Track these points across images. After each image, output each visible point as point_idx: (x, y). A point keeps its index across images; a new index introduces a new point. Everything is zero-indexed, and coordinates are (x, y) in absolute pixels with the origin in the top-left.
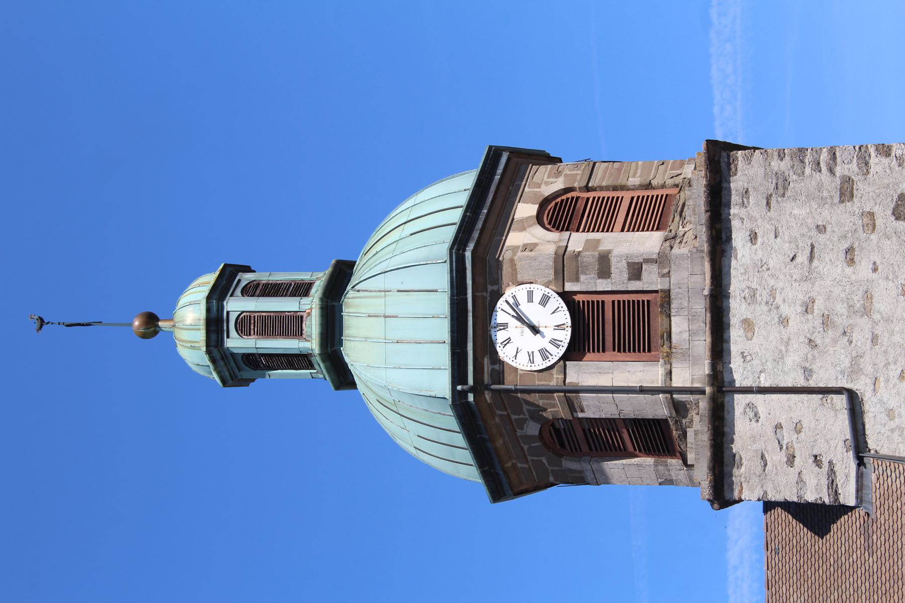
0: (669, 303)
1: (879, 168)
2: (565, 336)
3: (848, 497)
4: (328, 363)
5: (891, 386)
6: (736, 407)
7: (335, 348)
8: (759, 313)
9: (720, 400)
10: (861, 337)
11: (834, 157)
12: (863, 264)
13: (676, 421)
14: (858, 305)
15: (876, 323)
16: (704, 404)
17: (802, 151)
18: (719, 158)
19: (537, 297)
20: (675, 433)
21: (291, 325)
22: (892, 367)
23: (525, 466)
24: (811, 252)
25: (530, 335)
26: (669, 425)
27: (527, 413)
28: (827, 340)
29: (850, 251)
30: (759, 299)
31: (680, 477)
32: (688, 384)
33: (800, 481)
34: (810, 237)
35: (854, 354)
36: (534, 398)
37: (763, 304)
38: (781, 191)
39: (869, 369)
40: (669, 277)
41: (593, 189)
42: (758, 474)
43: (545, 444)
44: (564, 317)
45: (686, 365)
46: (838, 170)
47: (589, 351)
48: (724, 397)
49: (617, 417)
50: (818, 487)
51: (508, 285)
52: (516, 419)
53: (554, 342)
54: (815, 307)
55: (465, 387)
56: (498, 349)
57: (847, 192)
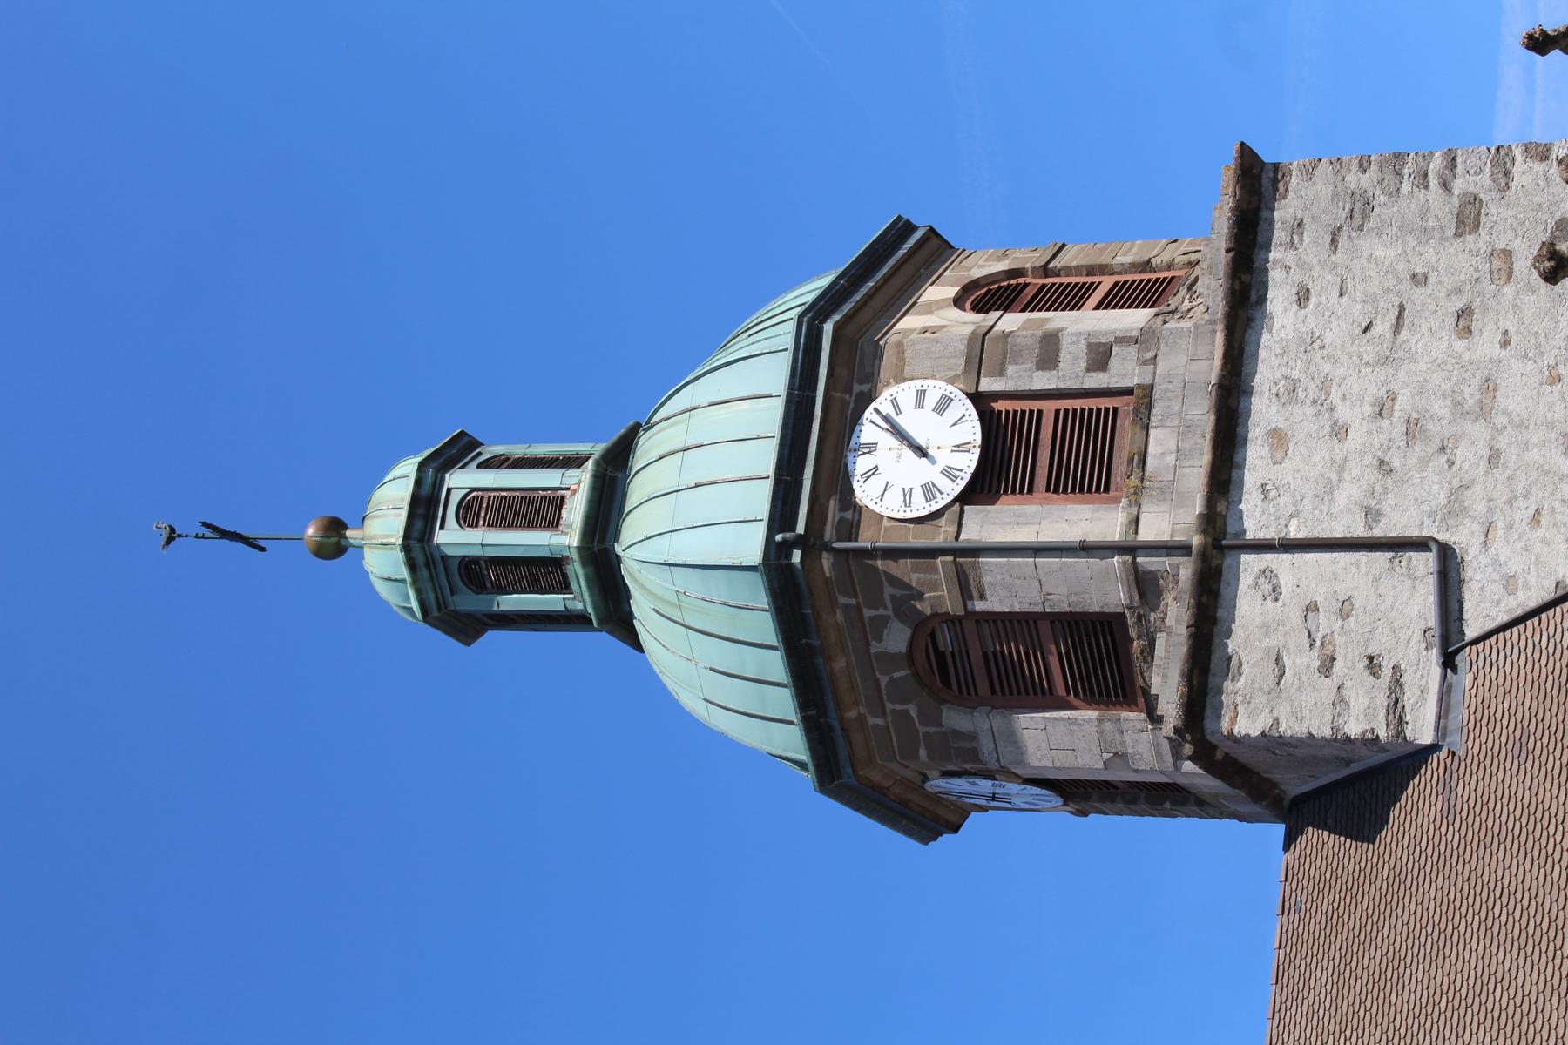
0: (1149, 407)
1: (1526, 180)
2: (968, 463)
3: (1422, 731)
5: (1516, 536)
6: (1242, 576)
8: (1302, 421)
9: (1215, 563)
10: (1469, 455)
11: (1452, 164)
12: (1485, 333)
13: (1140, 617)
14: (1471, 402)
15: (1499, 431)
16: (1186, 570)
17: (1399, 157)
18: (1256, 184)
19: (931, 400)
20: (1136, 646)
21: (541, 510)
22: (1521, 503)
23: (880, 721)
24: (1398, 318)
25: (918, 447)
26: (1126, 627)
27: (890, 605)
28: (1412, 461)
29: (1464, 314)
30: (1301, 395)
33: (1340, 700)
34: (1400, 293)
35: (1456, 483)
36: (903, 569)
38: (1357, 220)
39: (1479, 508)
42: (1266, 688)
43: (916, 674)
44: (972, 431)
45: (1165, 507)
46: (1458, 185)
47: (1006, 492)
48: (1223, 558)
49: (1039, 609)
50: (1369, 712)
52: (872, 618)
53: (949, 473)
54: (1397, 407)
55: (788, 535)
56: (855, 485)
57: (1469, 218)
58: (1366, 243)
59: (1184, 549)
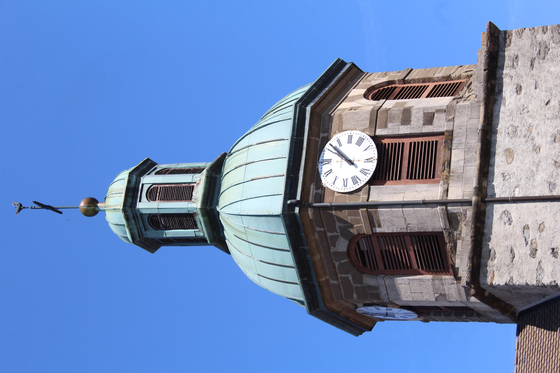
0: (451, 140)
2: (372, 167)
4: (206, 218)
6: (494, 214)
7: (213, 207)
8: (520, 145)
9: (482, 208)
13: (450, 233)
16: (470, 212)
18: (497, 40)
19: (355, 139)
20: (448, 246)
23: (335, 282)
27: (339, 231)
30: (519, 133)
31: (451, 292)
32: (460, 198)
33: (540, 268)
37: (522, 137)
38: (542, 55)
40: (454, 121)
41: (409, 82)
42: (507, 264)
43: (351, 261)
44: (373, 153)
47: (389, 179)
48: (486, 206)
49: (405, 231)
51: (335, 133)
52: (331, 237)
53: (363, 171)
55: (293, 201)
56: (322, 178)
58: (546, 65)
59: (469, 203)
